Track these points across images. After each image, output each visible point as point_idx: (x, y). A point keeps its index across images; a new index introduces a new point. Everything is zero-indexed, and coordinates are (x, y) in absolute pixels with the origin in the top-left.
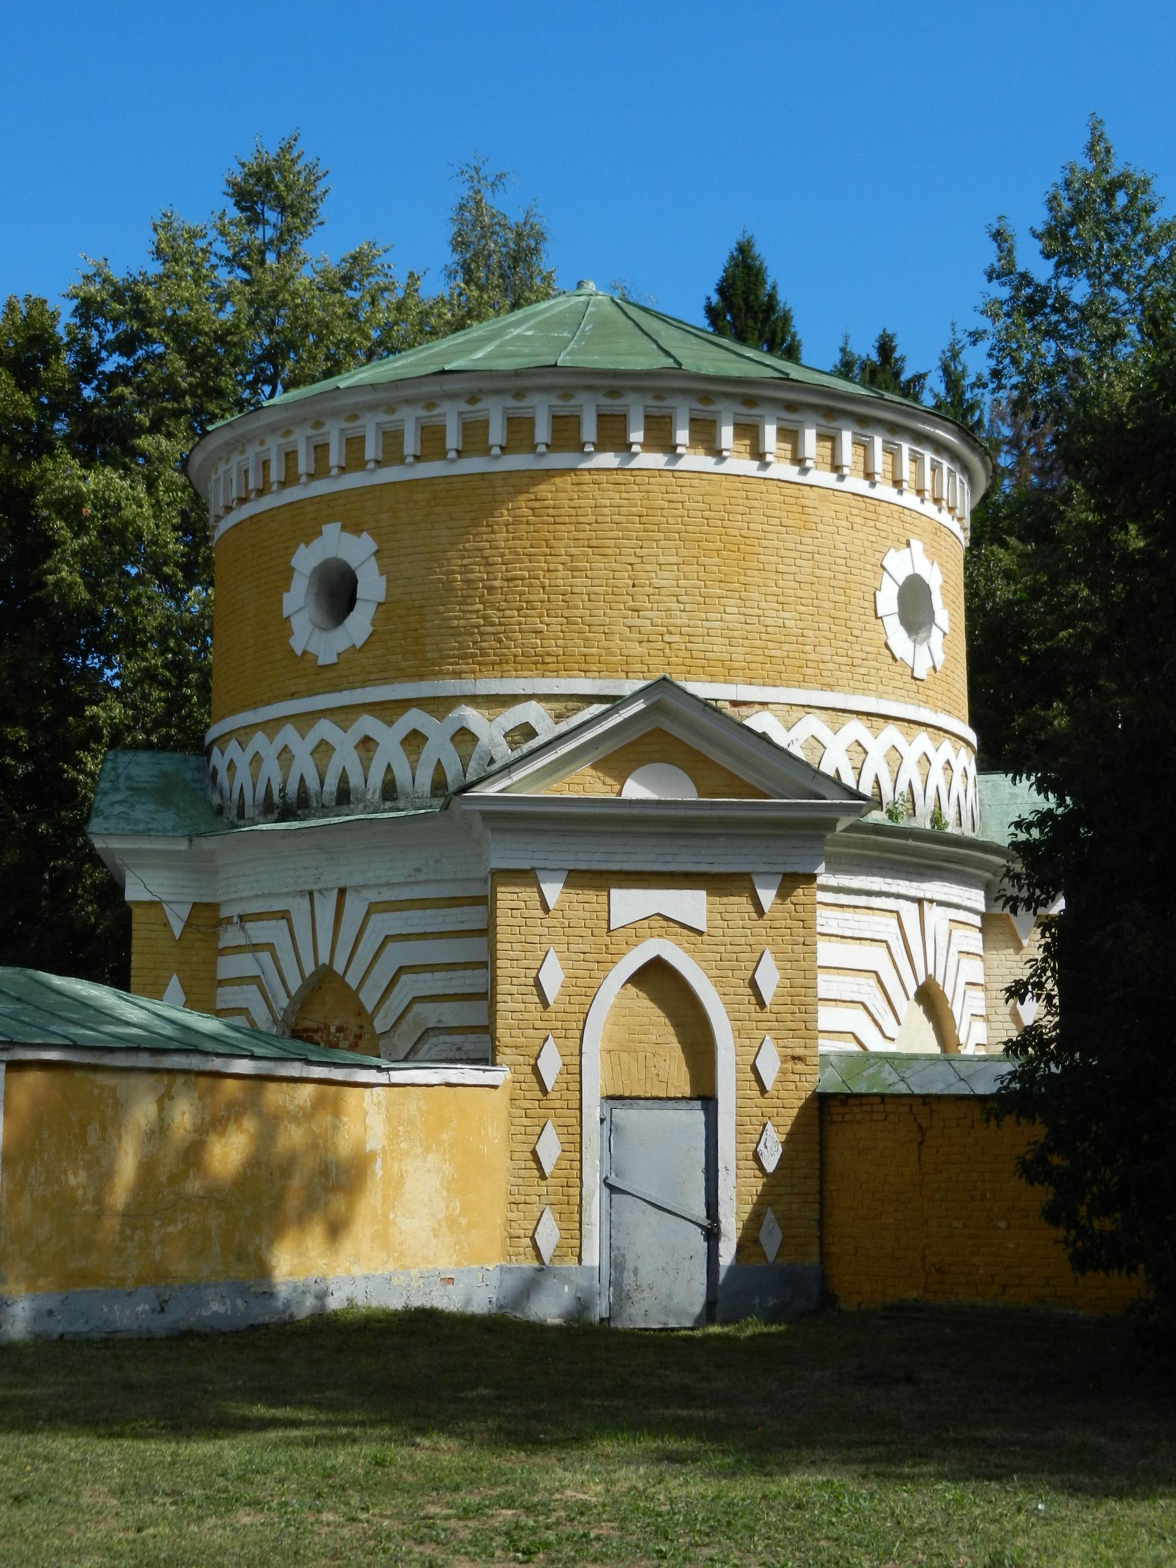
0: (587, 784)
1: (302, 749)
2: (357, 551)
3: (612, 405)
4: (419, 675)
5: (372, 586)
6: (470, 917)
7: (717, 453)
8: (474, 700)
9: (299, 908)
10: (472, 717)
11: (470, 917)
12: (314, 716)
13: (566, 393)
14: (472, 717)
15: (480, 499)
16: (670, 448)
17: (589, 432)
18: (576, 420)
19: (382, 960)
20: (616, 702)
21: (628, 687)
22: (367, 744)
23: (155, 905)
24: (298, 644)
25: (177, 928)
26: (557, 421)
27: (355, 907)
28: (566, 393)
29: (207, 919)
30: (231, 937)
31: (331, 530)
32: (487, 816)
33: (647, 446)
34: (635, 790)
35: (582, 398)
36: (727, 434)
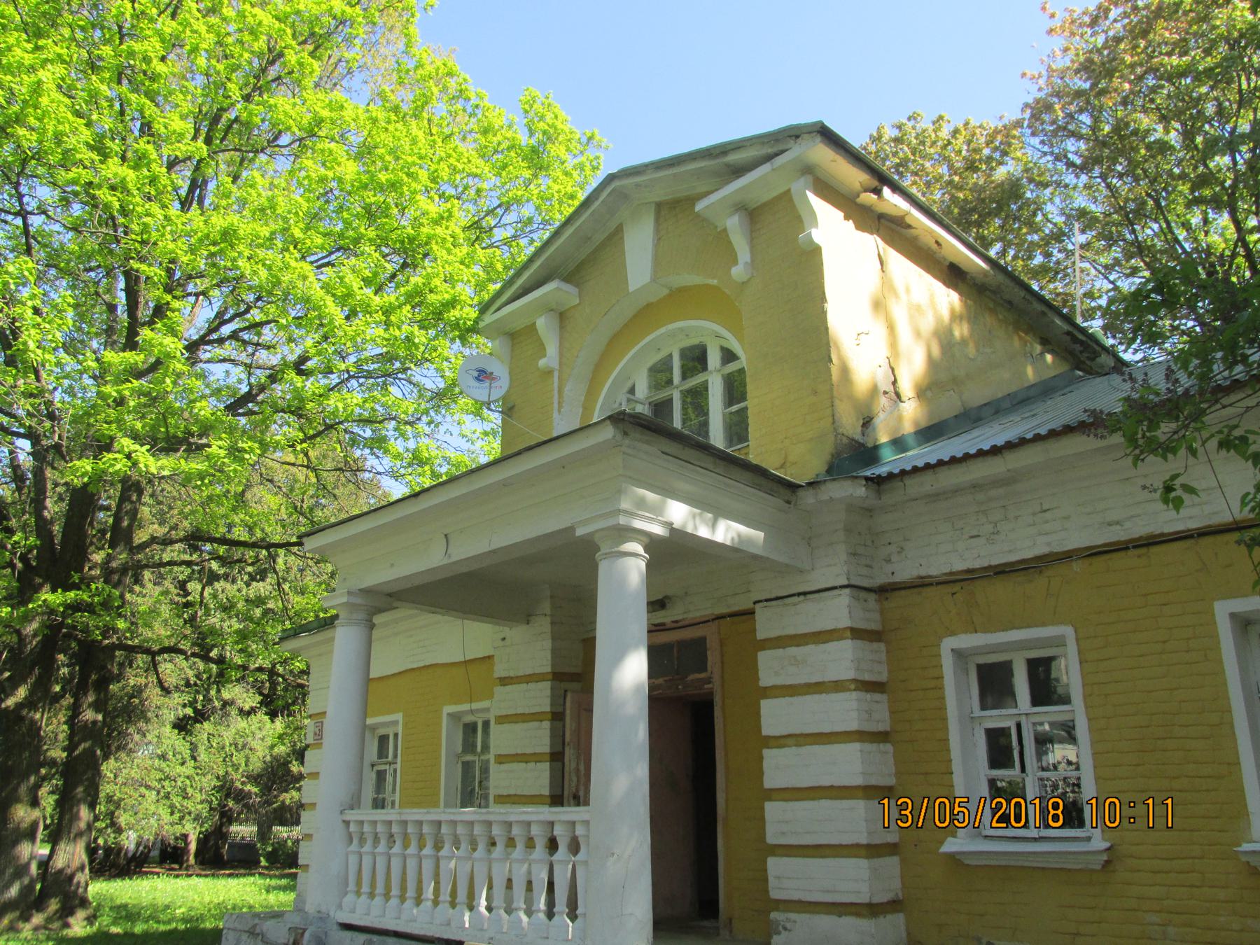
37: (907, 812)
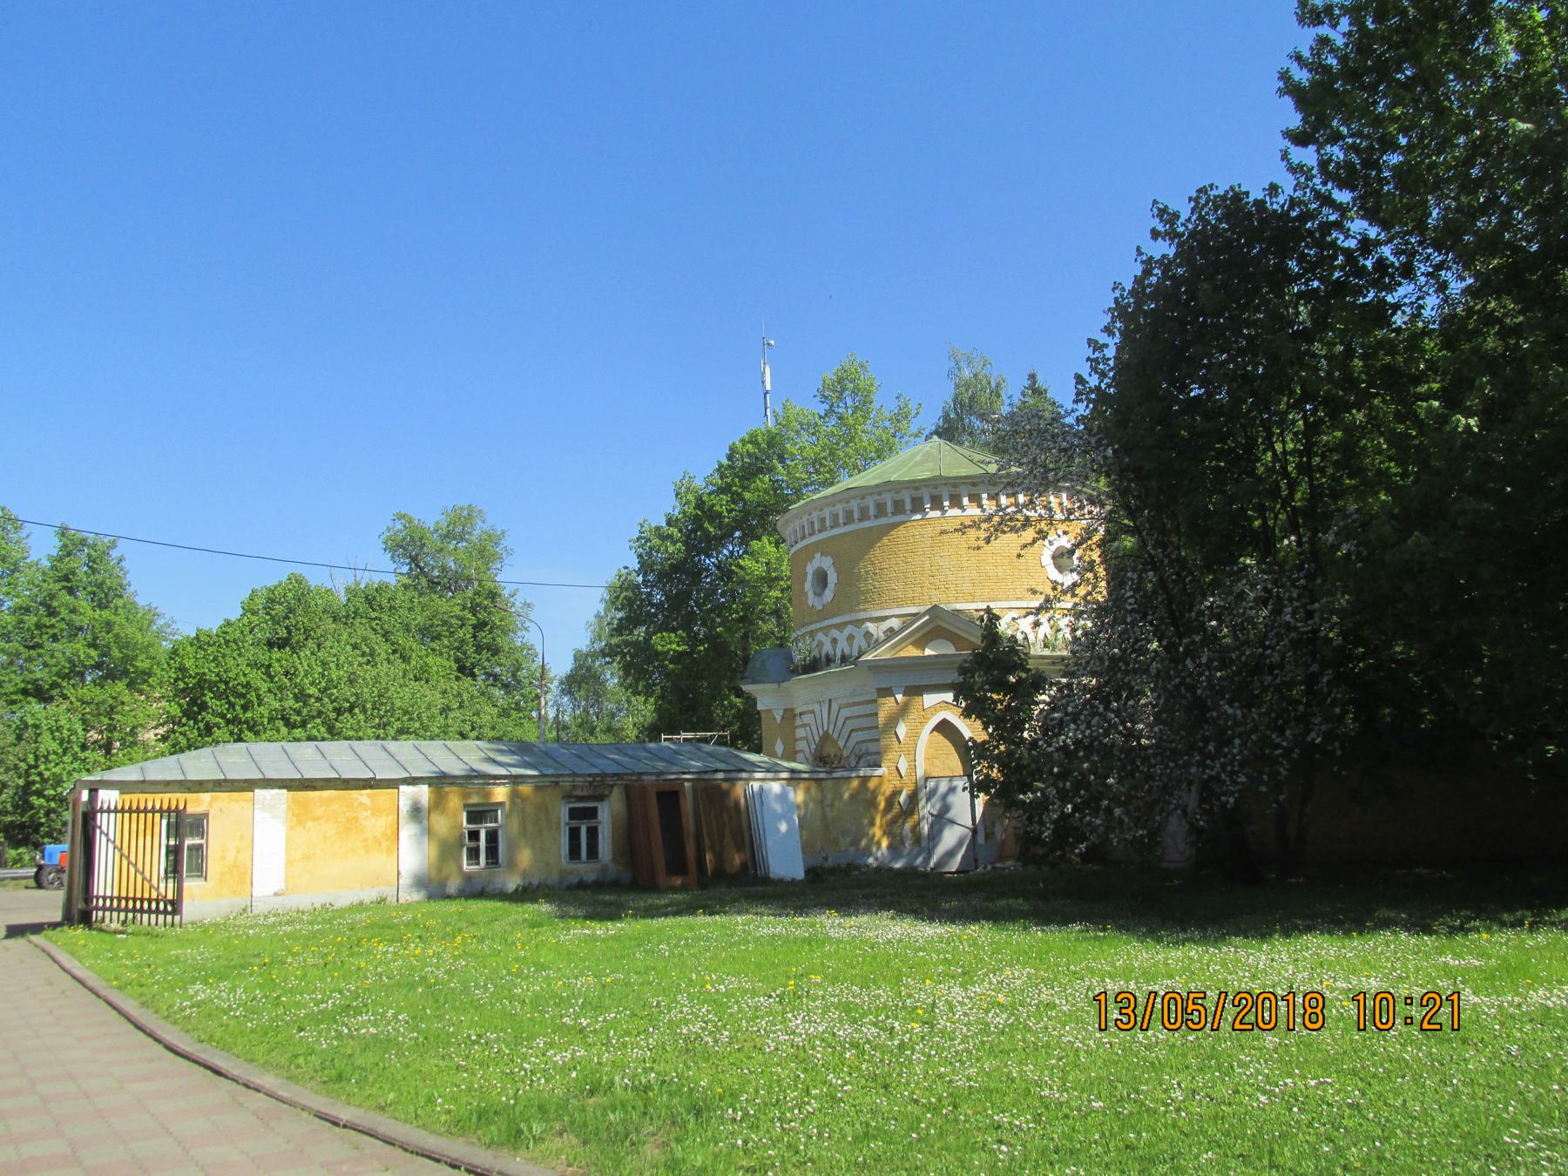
0: (912, 652)
1: (841, 637)
2: (826, 563)
3: (974, 490)
4: (852, 611)
5: (832, 578)
6: (868, 709)
7: (962, 508)
8: (872, 620)
9: (817, 708)
10: (871, 626)
11: (868, 709)
12: (845, 624)
13: (955, 486)
14: (871, 626)
15: (871, 538)
16: (941, 508)
17: (908, 506)
18: (921, 499)
19: (160, 1033)
20: (916, 616)
21: (923, 609)
22: (834, 641)
23: (769, 711)
24: (810, 603)
25: (779, 719)
26: (913, 500)
27: (835, 706)
28: (955, 486)
29: (790, 715)
30: (798, 722)
31: (818, 555)
32: (870, 668)
33: (951, 506)
34: (928, 652)
35: (962, 487)
36: (965, 501)
37: (1129, 1011)
